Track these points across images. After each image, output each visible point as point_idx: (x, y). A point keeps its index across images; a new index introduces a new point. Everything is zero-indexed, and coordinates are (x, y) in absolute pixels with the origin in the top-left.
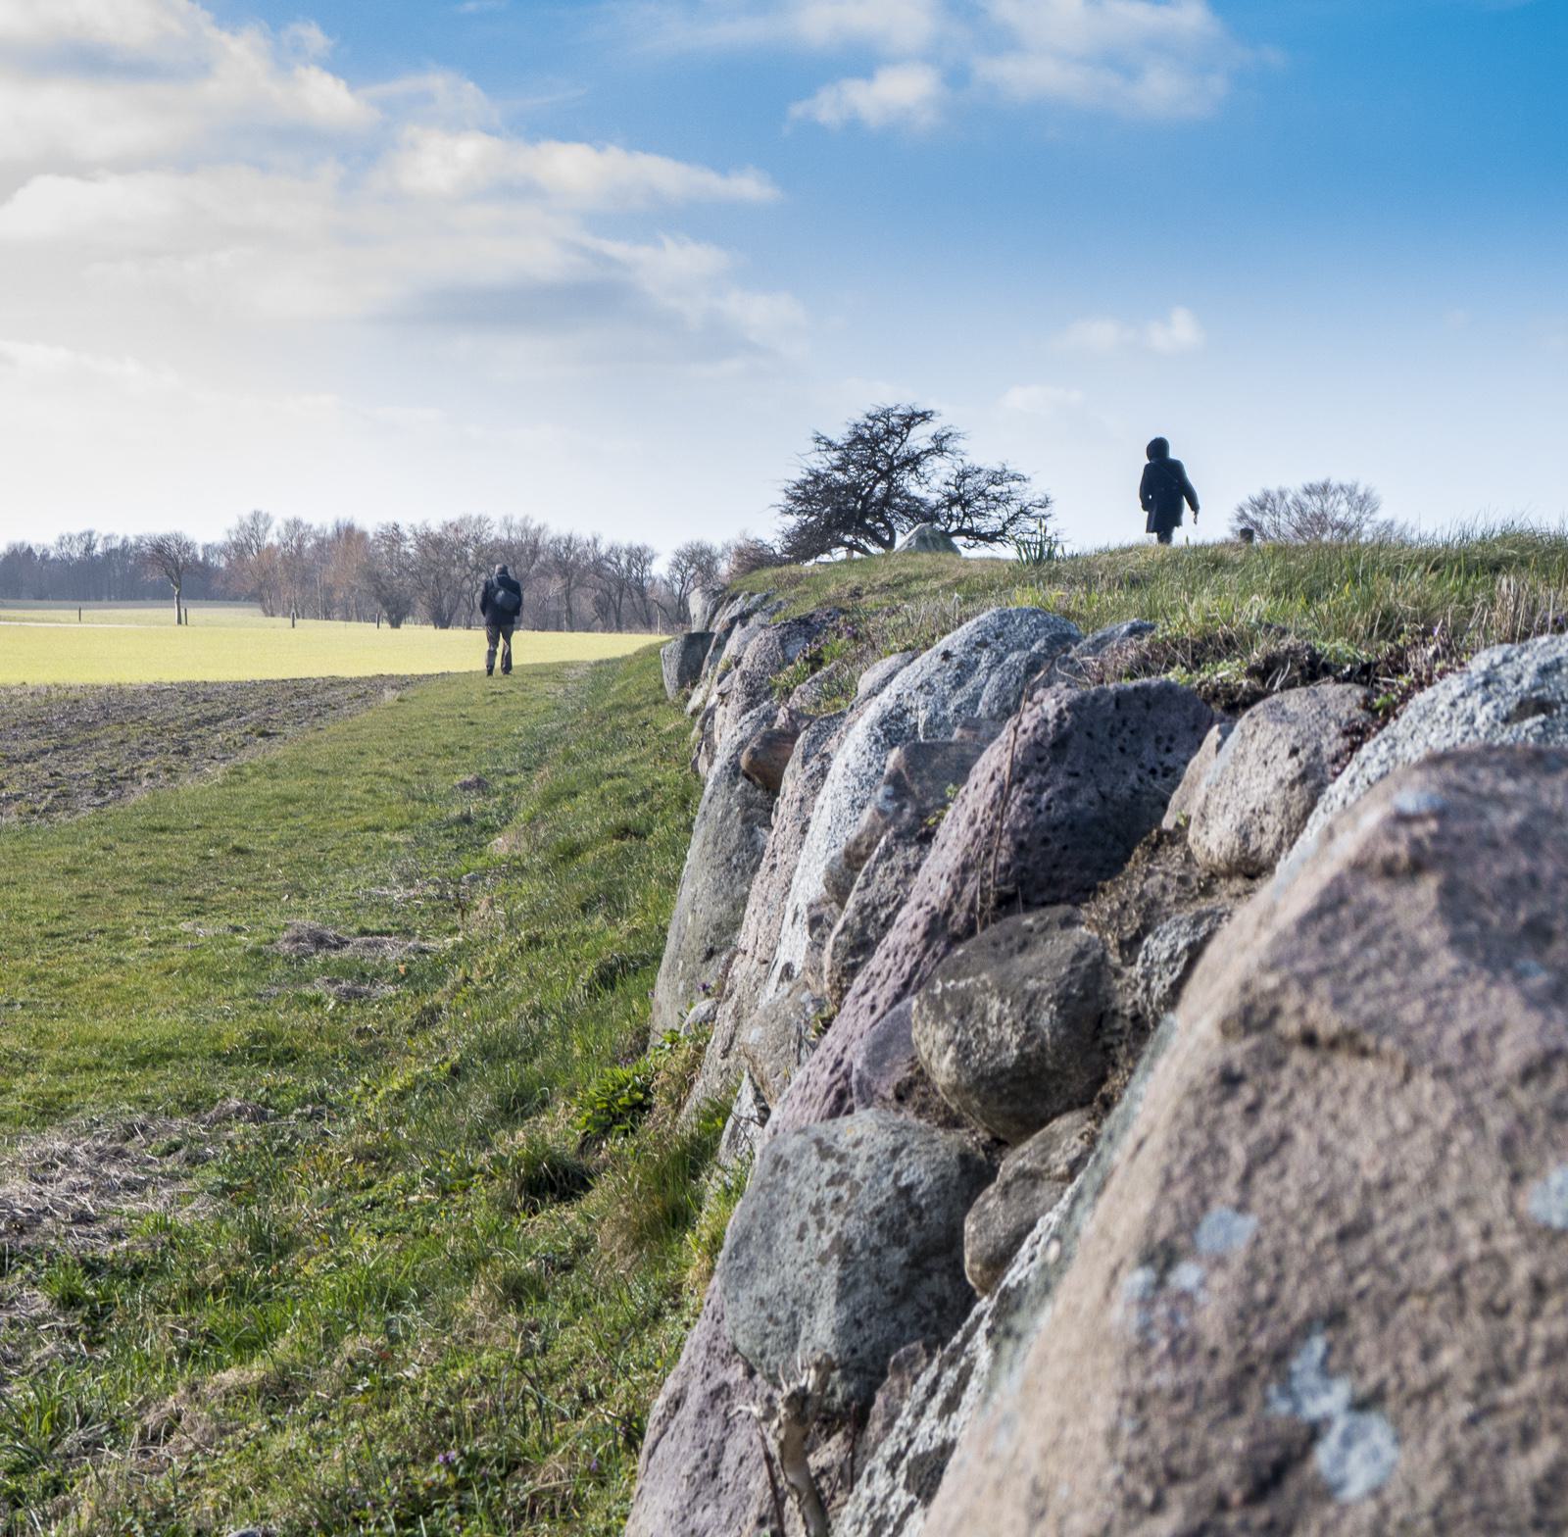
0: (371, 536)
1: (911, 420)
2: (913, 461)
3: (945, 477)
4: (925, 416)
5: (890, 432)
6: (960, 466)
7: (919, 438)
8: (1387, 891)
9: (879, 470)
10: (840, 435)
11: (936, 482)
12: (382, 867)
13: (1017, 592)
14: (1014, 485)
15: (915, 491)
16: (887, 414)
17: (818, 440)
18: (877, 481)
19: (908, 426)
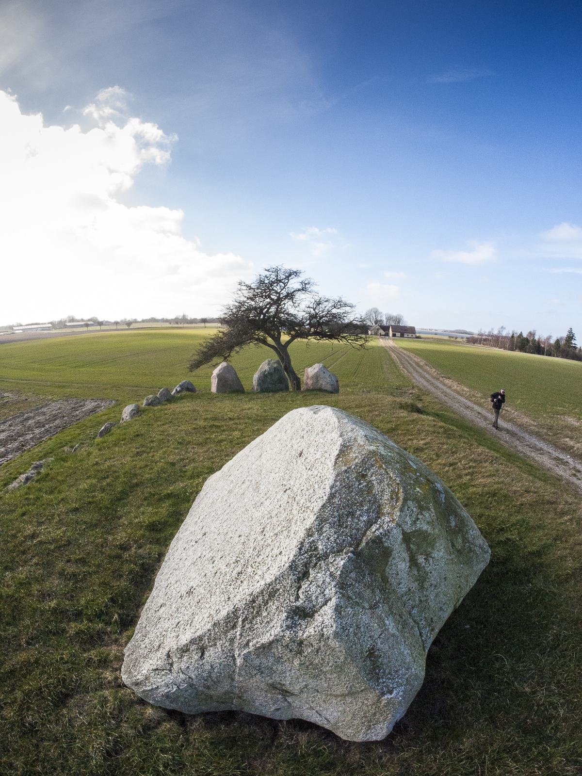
0: (170, 152)
1: (290, 274)
2: (290, 296)
3: (308, 304)
4: (296, 273)
5: (278, 281)
6: (317, 299)
7: (294, 284)
8: (481, 568)
9: (272, 299)
10: (252, 281)
11: (303, 306)
12: (192, 544)
13: (17, 485)
14: (348, 309)
15: (292, 311)
16: (277, 271)
17: (240, 284)
18: (271, 305)
19: (288, 278)
